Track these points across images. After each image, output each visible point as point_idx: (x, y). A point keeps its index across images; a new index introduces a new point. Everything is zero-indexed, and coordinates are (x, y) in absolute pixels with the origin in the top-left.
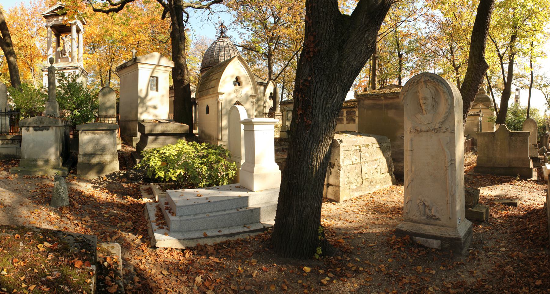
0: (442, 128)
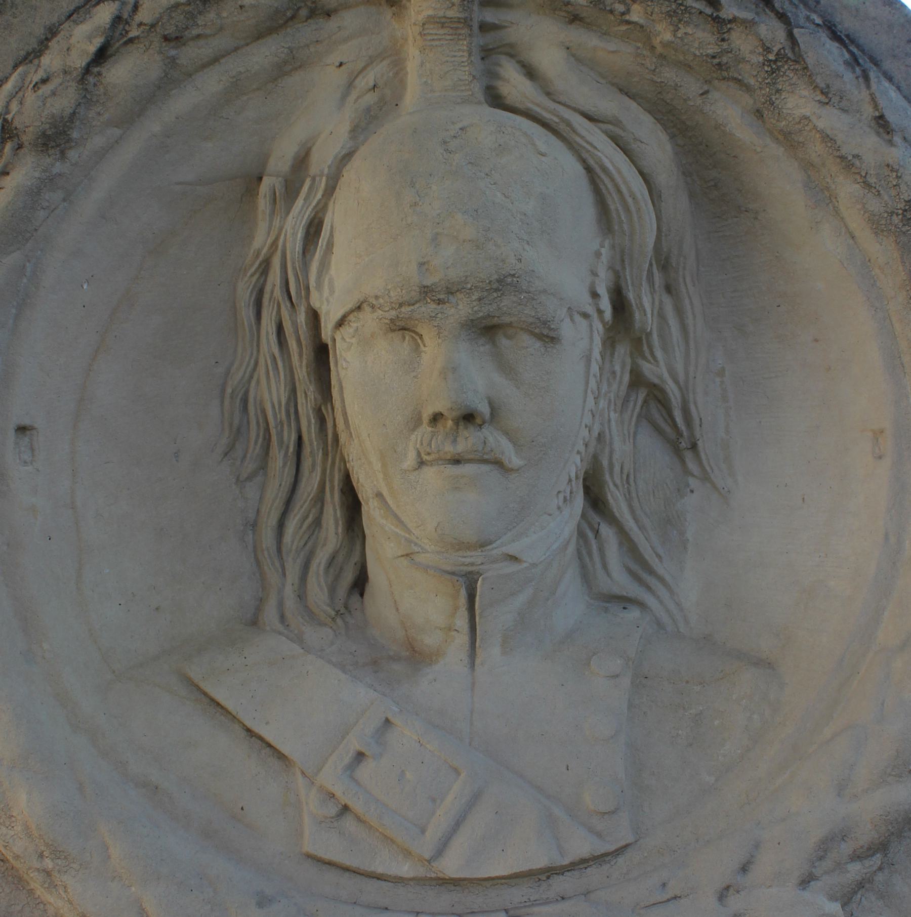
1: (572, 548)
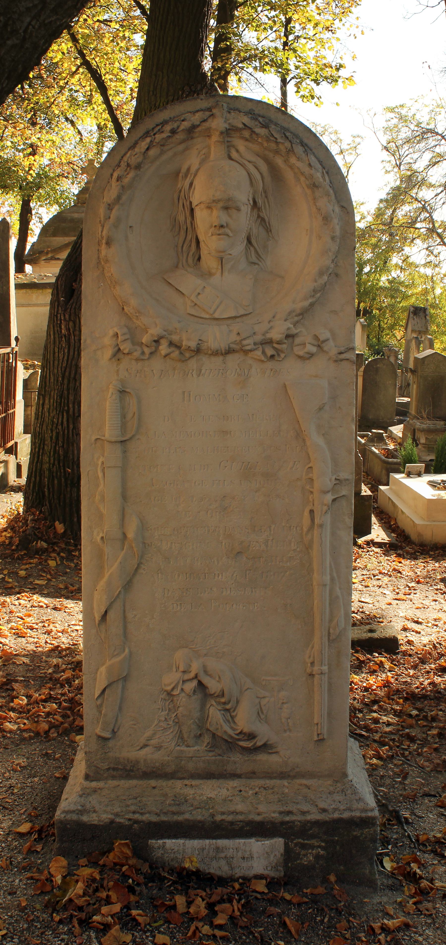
0: (297, 341)
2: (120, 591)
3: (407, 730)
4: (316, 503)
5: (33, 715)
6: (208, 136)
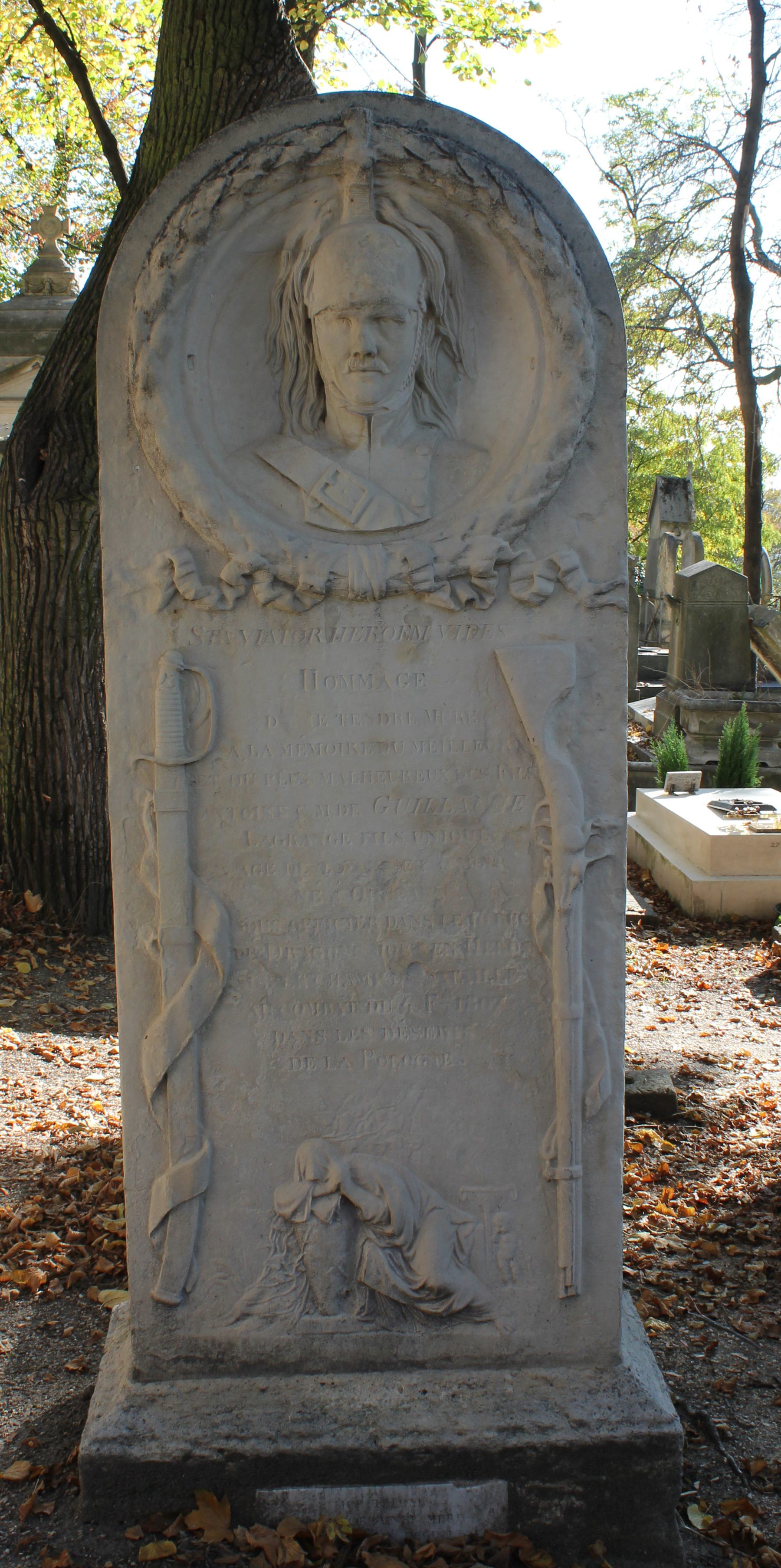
0: (517, 571)
1: (410, 404)
2: (191, 1039)
3: (706, 1263)
4: (556, 870)
5: (14, 1254)
6: (337, 175)
